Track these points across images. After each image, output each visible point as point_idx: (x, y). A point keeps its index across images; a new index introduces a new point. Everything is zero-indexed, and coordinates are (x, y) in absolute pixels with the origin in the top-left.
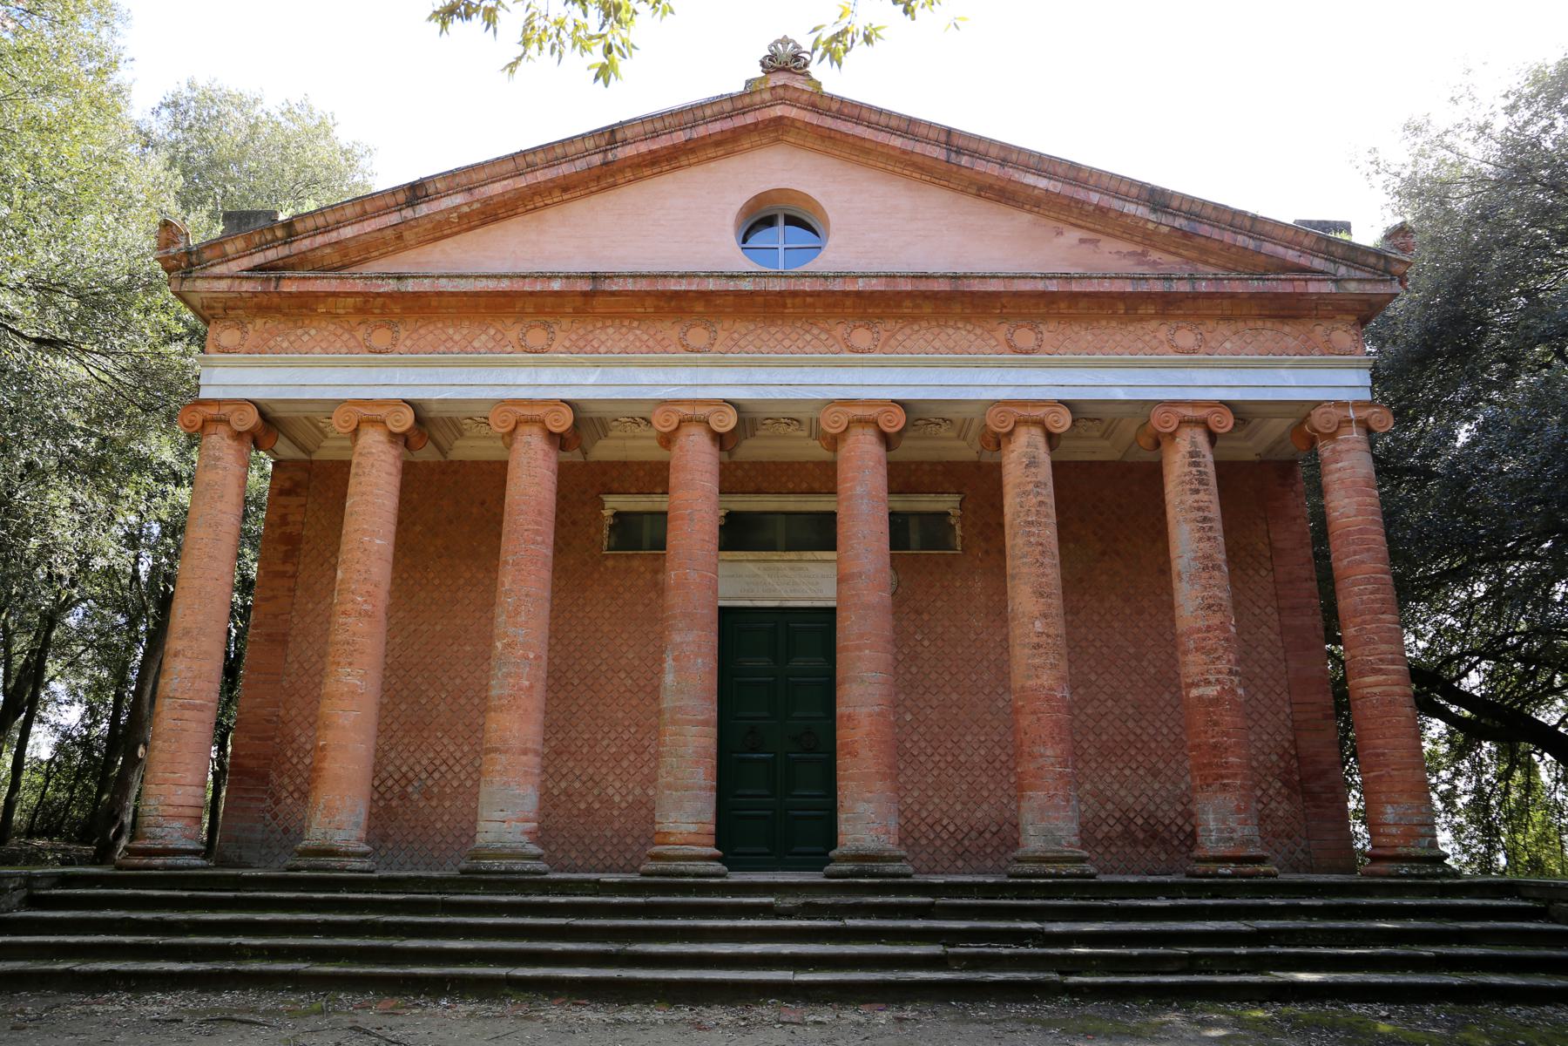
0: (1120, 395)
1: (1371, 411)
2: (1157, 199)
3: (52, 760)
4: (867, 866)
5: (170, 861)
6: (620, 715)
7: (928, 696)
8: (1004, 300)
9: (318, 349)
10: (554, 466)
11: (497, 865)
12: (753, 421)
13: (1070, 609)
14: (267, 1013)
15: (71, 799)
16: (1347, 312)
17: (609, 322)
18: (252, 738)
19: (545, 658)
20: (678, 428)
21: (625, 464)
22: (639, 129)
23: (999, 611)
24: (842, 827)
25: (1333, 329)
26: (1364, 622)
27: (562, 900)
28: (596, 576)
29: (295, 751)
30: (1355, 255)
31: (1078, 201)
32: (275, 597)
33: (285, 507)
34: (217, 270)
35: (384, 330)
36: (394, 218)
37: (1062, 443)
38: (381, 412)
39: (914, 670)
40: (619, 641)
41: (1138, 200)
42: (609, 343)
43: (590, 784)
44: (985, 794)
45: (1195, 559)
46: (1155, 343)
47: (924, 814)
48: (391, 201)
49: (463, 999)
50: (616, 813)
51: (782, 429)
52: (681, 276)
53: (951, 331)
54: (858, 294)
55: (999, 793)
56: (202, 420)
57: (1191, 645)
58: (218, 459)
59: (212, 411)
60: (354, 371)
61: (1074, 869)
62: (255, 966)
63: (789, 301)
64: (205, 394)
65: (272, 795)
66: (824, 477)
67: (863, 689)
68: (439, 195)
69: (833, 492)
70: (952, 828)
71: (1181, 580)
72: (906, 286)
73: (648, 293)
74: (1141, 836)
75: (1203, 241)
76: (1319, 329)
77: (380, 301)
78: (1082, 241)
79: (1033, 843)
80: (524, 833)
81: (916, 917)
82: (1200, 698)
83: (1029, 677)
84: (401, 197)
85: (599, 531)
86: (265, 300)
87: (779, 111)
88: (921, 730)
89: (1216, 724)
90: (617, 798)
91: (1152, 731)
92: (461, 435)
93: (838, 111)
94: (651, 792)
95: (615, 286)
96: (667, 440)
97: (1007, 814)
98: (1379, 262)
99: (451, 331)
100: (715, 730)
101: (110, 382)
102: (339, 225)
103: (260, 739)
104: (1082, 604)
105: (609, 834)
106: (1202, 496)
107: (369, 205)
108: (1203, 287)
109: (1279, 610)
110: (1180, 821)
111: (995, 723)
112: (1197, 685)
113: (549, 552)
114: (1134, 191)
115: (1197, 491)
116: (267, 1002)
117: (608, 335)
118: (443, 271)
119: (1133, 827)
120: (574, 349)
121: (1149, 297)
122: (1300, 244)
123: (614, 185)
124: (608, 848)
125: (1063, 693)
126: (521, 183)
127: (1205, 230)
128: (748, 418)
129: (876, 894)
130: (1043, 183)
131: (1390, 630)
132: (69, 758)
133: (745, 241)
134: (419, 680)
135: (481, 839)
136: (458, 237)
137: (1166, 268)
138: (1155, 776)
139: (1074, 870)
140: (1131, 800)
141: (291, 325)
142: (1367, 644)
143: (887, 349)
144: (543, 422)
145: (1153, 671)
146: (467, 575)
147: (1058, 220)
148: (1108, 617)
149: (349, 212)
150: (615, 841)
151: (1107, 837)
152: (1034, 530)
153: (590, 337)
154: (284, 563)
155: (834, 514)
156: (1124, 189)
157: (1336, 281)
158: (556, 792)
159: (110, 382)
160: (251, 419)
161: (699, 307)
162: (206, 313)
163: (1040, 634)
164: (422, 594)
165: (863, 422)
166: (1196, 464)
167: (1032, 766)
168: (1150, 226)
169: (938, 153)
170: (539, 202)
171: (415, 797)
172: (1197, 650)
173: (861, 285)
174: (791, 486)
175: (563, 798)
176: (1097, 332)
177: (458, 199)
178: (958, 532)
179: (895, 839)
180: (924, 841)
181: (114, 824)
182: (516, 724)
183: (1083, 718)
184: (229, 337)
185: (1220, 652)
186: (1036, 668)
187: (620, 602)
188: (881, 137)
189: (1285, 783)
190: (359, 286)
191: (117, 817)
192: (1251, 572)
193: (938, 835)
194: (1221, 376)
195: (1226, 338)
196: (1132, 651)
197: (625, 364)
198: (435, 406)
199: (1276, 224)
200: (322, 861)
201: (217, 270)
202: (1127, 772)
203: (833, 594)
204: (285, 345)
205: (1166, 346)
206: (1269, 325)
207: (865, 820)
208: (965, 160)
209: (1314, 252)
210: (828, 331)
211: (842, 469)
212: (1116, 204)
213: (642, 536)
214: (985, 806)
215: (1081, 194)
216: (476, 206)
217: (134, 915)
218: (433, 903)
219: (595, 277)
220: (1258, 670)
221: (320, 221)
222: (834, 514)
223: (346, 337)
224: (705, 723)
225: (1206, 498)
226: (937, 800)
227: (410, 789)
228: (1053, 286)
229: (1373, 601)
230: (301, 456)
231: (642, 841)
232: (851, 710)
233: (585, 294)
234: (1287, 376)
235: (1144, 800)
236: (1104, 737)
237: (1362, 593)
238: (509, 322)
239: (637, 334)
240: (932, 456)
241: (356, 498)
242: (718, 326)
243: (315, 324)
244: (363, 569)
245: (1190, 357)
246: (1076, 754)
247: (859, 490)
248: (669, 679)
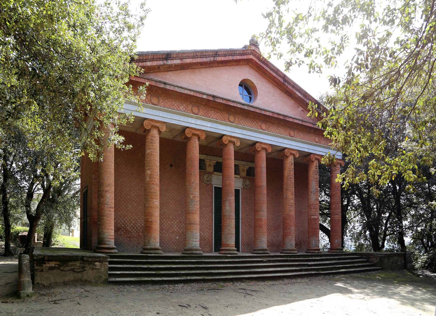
17: (212, 109)
22: (222, 53)
42: (213, 115)
48: (161, 57)
57: (313, 207)
78: (302, 111)
82: (314, 218)
87: (251, 57)
112: (313, 216)
117: (212, 113)
123: (212, 67)
130: (299, 95)
136: (174, 72)
169: (281, 80)
173: (267, 113)
188: (271, 72)
208: (286, 84)
210: (257, 123)
237: (337, 199)
245: (196, 115)
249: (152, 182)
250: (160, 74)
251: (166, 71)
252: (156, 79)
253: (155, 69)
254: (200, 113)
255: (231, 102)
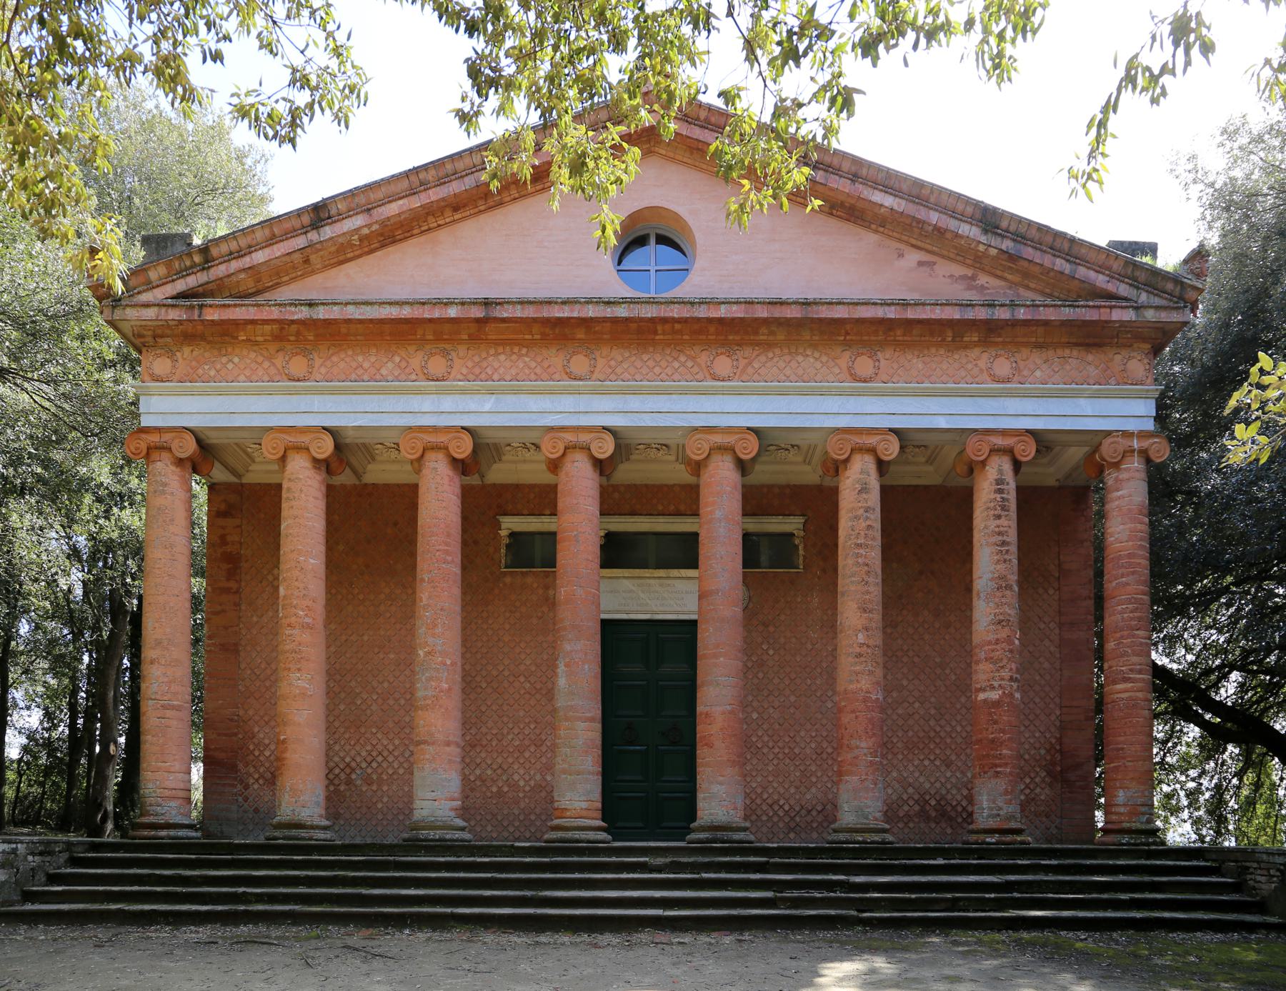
0: (942, 423)
1: (1151, 441)
2: (989, 218)
3: (20, 760)
4: (719, 834)
5: (172, 833)
6: (522, 713)
7: (771, 698)
8: (848, 327)
9: (242, 378)
10: (458, 490)
11: (432, 834)
12: (628, 446)
13: (889, 624)
14: (276, 938)
15: (44, 793)
16: (1144, 339)
17: (500, 349)
18: (219, 735)
19: (459, 664)
20: (564, 454)
21: (517, 487)
23: (831, 625)
24: (701, 804)
25: (1130, 358)
26: (1122, 637)
27: (487, 860)
28: (496, 591)
29: (257, 746)
30: (1155, 280)
31: (919, 221)
32: (224, 611)
33: (223, 528)
34: (145, 297)
35: (299, 358)
36: (300, 242)
37: (892, 468)
38: (305, 439)
39: (761, 675)
40: (518, 650)
41: (971, 220)
42: (502, 370)
43: (499, 771)
44: (814, 780)
45: (991, 580)
46: (976, 371)
47: (765, 796)
48: (296, 223)
49: (420, 929)
50: (521, 795)
51: (653, 454)
52: (564, 303)
53: (800, 358)
54: (721, 321)
55: (825, 779)
56: (143, 446)
57: (982, 655)
58: (165, 485)
59: (154, 438)
60: (277, 399)
61: (877, 838)
62: (260, 907)
63: (659, 328)
64: (146, 421)
65: (242, 781)
66: (686, 499)
67: (718, 690)
68: (342, 217)
69: (696, 514)
70: (787, 807)
71: (979, 598)
72: (762, 313)
73: (535, 320)
74: (934, 814)
75: (1026, 264)
76: (1118, 357)
77: (294, 327)
79: (847, 817)
80: (452, 809)
81: (755, 872)
82: (985, 701)
83: (851, 682)
84: (306, 219)
85: (497, 550)
86: (189, 328)
88: (765, 727)
89: (996, 722)
90: (522, 783)
91: (948, 729)
92: (373, 459)
93: (707, 120)
94: (549, 778)
95: (505, 313)
96: (555, 466)
97: (830, 796)
98: (1173, 289)
99: (360, 359)
100: (600, 726)
101: (53, 409)
102: (250, 249)
103: (226, 735)
104: (900, 619)
105: (516, 812)
106: (1003, 522)
107: (277, 228)
108: (1022, 314)
109: (1061, 625)
110: (964, 803)
111: (824, 722)
112: (984, 690)
113: (458, 570)
114: (969, 210)
115: (999, 517)
116: (275, 932)
117: (501, 362)
118: (349, 297)
119: (928, 808)
120: (471, 377)
121: (973, 324)
122: (1109, 269)
124: (517, 824)
125: (877, 695)
126: (415, 202)
127: (1028, 252)
128: (624, 443)
129: (726, 855)
130: (889, 201)
131: (1141, 644)
132: (36, 758)
133: (619, 263)
134: (353, 684)
135: (418, 815)
137: (991, 294)
138: (948, 766)
139: (876, 839)
140: (927, 785)
141: (216, 352)
142: (1122, 656)
143: (745, 377)
144: (446, 448)
145: (953, 677)
146: (387, 591)
147: (900, 240)
148: (921, 629)
149: (259, 235)
150: (522, 818)
151: (907, 815)
152: (862, 551)
153: (484, 364)
154: (228, 580)
155: (696, 535)
156: (960, 207)
157: (1137, 308)
158: (472, 778)
159: (53, 409)
160: (189, 447)
161: (581, 334)
162: (138, 342)
163: (861, 645)
164: (350, 608)
165: (723, 449)
166: (1000, 491)
167: (849, 756)
168: (981, 248)
170: (432, 222)
171: (359, 782)
172: (986, 659)
173: (723, 312)
174: (660, 508)
175: (478, 783)
176: (927, 359)
177: (358, 221)
178: (801, 552)
179: (741, 814)
180: (764, 818)
181: (99, 810)
182: (439, 720)
183: (895, 717)
184: (161, 365)
185: (1005, 661)
186: (857, 673)
187: (518, 615)
189: (1049, 773)
190: (275, 313)
191: (100, 805)
192: (1041, 591)
193: (776, 813)
194: (1029, 405)
195: (1037, 365)
196: (938, 660)
197: (517, 391)
198: (351, 433)
199: (1092, 246)
200: (294, 832)
201: (145, 297)
202: (926, 762)
203: (695, 608)
204: (212, 373)
205: (985, 376)
206: (1075, 353)
207: (718, 799)
209: (1121, 277)
210: (693, 358)
211: (704, 492)
212: (952, 224)
213: (535, 553)
214: (814, 790)
215: (922, 213)
216: (375, 227)
217: (158, 872)
218: (388, 862)
219: (487, 303)
220: (1038, 678)
221: (233, 246)
222: (696, 535)
223: (266, 364)
224: (592, 720)
225: (1006, 523)
226: (775, 785)
227: (354, 776)
228: (891, 313)
229: (1132, 619)
230: (233, 479)
231: (543, 817)
232: (708, 709)
233: (478, 320)
234: (1085, 406)
235: (938, 785)
236: (910, 733)
238: (411, 349)
239: (526, 361)
240: (782, 480)
241: (290, 521)
242: (597, 354)
243: (237, 351)
244: (301, 586)
245: (1005, 386)
246: (885, 747)
247: (718, 514)
248: (562, 682)
250: (317, 279)
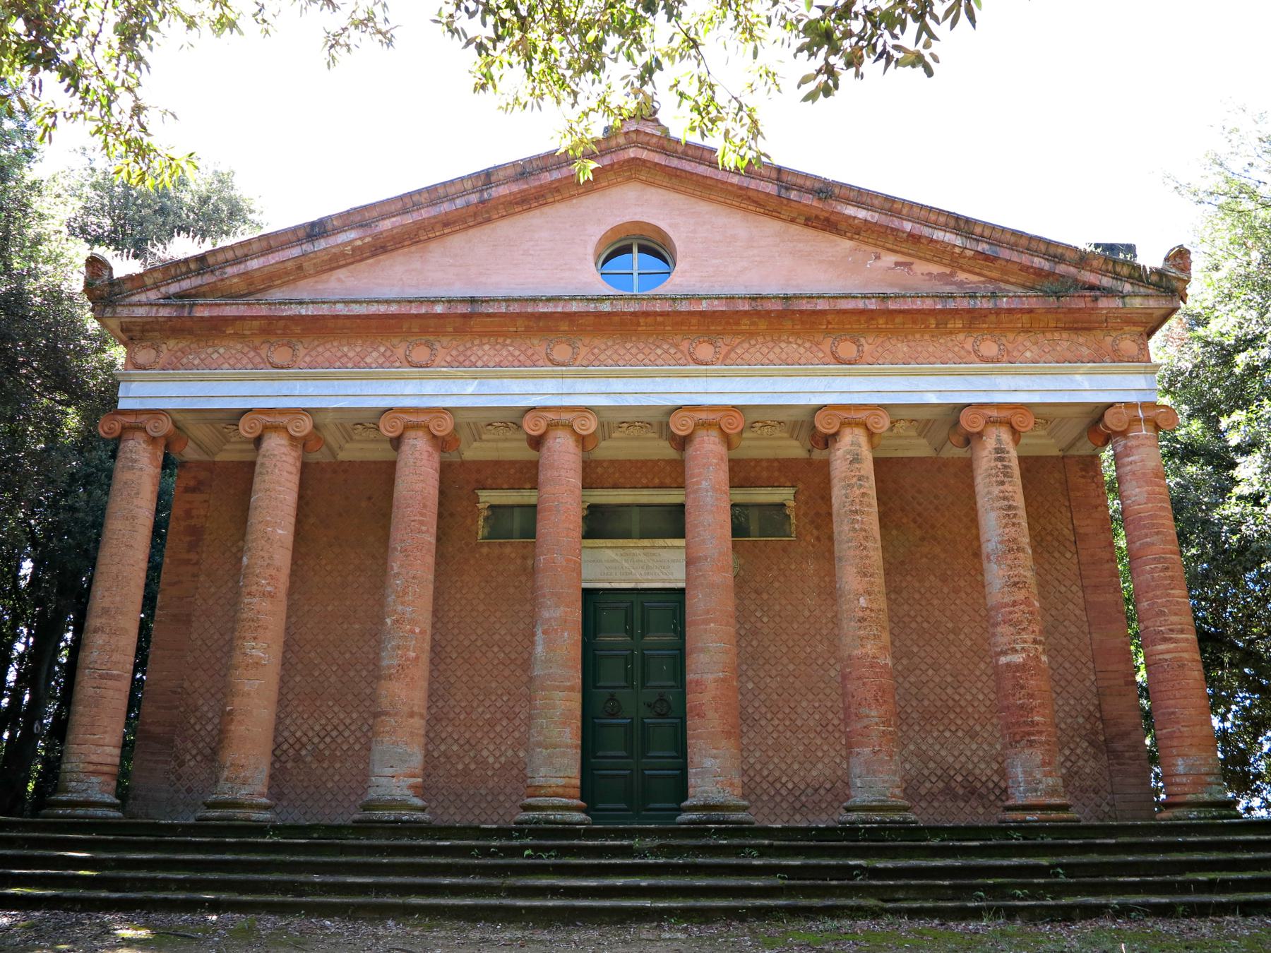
82: (1008, 665)
87: (632, 153)
112: (1004, 653)
117: (485, 350)
123: (489, 220)
130: (862, 214)
210: (676, 346)
249: (248, 589)
251: (325, 271)
252: (296, 296)
253: (287, 273)
254: (438, 360)
255: (541, 304)
